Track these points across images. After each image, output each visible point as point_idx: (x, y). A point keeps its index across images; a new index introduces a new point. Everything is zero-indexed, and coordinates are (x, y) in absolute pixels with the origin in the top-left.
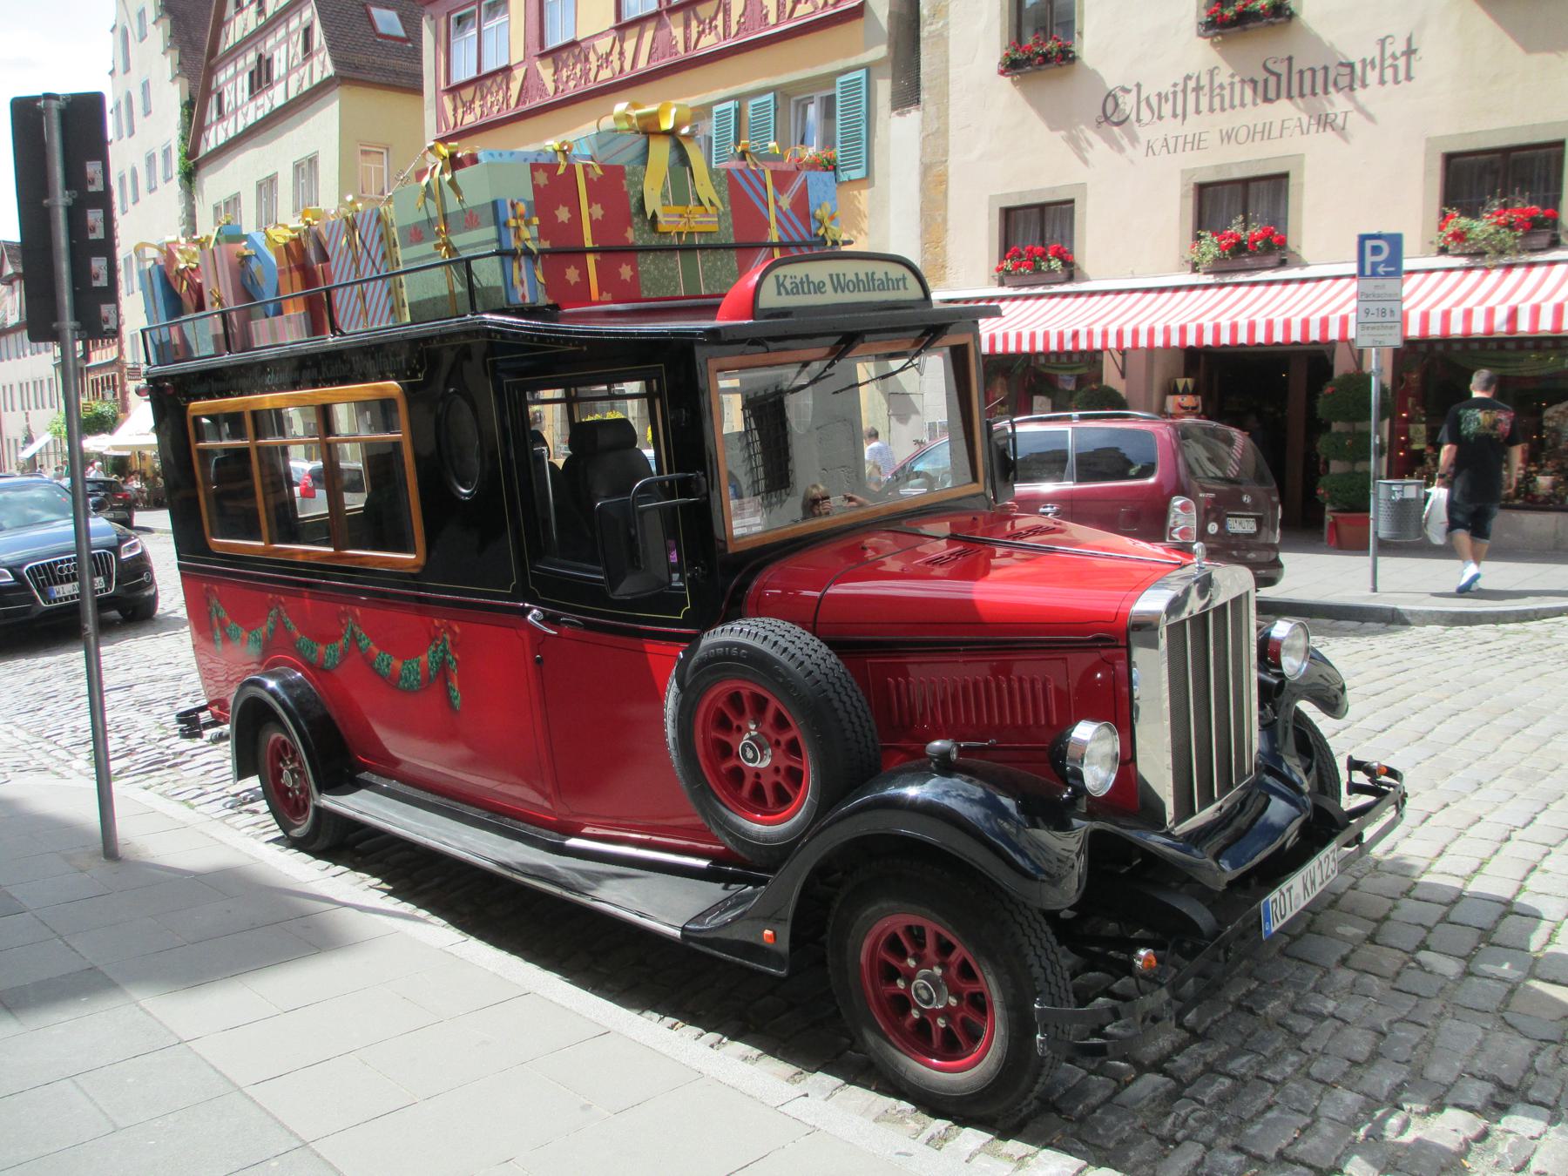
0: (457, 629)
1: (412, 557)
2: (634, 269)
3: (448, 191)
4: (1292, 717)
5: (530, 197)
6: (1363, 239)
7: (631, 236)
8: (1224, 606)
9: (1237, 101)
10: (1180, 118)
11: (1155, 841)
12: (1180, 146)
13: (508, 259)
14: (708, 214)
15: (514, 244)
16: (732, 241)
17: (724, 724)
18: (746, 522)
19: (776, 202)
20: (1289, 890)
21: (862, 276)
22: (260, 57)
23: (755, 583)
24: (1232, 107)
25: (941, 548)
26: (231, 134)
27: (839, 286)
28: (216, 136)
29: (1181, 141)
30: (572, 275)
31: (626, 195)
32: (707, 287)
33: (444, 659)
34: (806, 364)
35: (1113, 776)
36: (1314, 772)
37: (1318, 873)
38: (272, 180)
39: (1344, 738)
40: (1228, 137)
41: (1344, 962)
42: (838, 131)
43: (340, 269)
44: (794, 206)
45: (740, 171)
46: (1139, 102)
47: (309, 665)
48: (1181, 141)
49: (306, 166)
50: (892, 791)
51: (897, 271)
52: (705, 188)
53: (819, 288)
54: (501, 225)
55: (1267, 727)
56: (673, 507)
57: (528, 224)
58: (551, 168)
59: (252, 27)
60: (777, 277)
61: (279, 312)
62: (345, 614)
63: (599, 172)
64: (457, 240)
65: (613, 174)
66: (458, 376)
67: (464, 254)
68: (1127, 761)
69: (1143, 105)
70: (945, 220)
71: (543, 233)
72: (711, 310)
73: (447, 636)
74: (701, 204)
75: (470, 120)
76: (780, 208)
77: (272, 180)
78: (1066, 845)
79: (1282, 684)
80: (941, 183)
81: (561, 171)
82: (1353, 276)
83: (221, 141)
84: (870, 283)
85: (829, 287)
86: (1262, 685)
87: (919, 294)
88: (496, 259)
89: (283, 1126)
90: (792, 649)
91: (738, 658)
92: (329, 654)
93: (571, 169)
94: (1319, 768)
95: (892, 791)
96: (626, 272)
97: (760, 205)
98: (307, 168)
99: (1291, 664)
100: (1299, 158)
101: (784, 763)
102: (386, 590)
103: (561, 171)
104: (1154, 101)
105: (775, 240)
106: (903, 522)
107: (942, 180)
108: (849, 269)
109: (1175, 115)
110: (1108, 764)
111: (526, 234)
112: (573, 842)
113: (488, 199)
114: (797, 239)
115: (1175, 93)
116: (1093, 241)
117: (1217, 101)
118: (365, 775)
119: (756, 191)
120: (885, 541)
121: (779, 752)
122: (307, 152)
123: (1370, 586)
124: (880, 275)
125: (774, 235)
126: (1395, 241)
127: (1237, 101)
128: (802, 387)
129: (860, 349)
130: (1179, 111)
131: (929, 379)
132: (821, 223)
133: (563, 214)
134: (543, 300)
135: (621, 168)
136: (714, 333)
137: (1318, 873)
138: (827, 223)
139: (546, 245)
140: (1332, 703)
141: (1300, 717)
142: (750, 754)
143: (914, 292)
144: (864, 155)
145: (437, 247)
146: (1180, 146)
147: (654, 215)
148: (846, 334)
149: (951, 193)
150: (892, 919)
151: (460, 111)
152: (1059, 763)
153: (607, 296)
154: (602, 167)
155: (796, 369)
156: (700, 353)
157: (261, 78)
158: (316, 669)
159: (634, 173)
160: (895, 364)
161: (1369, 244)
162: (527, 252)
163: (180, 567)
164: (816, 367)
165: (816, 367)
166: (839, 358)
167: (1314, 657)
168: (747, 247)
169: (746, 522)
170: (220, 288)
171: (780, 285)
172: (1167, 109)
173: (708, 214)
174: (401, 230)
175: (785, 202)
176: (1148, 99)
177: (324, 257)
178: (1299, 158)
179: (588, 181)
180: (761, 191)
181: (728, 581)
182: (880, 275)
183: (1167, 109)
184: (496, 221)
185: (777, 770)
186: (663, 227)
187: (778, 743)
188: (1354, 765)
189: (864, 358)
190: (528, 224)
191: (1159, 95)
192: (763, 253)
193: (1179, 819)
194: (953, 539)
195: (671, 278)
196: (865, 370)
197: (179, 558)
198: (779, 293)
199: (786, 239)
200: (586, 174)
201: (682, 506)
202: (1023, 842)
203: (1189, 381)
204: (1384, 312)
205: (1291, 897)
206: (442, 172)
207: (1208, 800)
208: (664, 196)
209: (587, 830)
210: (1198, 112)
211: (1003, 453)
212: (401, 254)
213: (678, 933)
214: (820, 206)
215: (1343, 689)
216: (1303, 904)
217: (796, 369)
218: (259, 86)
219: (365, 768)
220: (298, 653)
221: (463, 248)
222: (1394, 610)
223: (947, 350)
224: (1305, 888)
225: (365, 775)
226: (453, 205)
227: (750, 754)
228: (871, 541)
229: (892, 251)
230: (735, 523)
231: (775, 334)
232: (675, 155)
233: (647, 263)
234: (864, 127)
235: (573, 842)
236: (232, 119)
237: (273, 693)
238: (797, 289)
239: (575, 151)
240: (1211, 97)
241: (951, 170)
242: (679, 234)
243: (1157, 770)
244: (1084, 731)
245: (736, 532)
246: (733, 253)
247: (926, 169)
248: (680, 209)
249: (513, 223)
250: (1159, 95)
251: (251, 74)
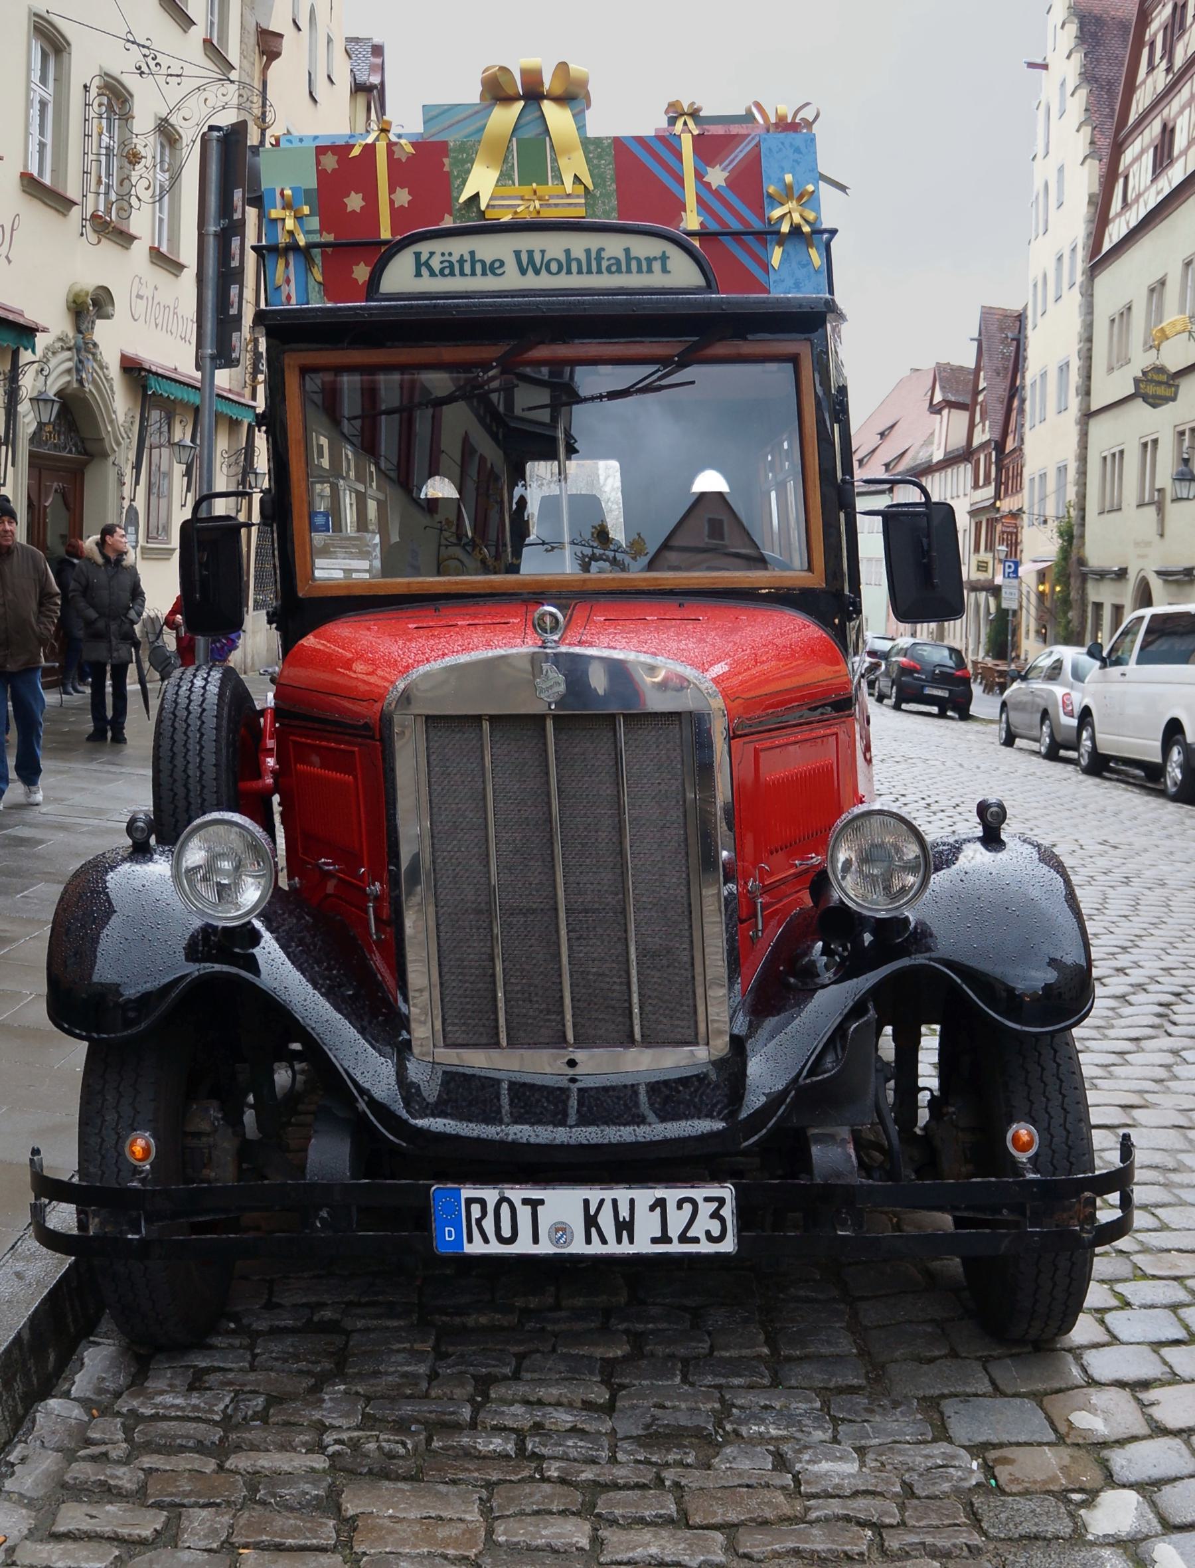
5: (313, 184)
19: (699, 176)
22: (1165, 126)
28: (1116, 231)
44: (731, 183)
53: (494, 268)
58: (341, 150)
59: (1160, 87)
60: (418, 255)
89: (1138, 1343)
93: (370, 149)
103: (356, 152)
114: (736, 226)
133: (355, 202)
135: (445, 144)
139: (329, 238)
154: (414, 145)
157: (1163, 155)
162: (293, 247)
175: (717, 177)
198: (418, 274)
199: (713, 227)
202: (422, 936)
218: (1161, 165)
238: (449, 270)
251: (1156, 148)
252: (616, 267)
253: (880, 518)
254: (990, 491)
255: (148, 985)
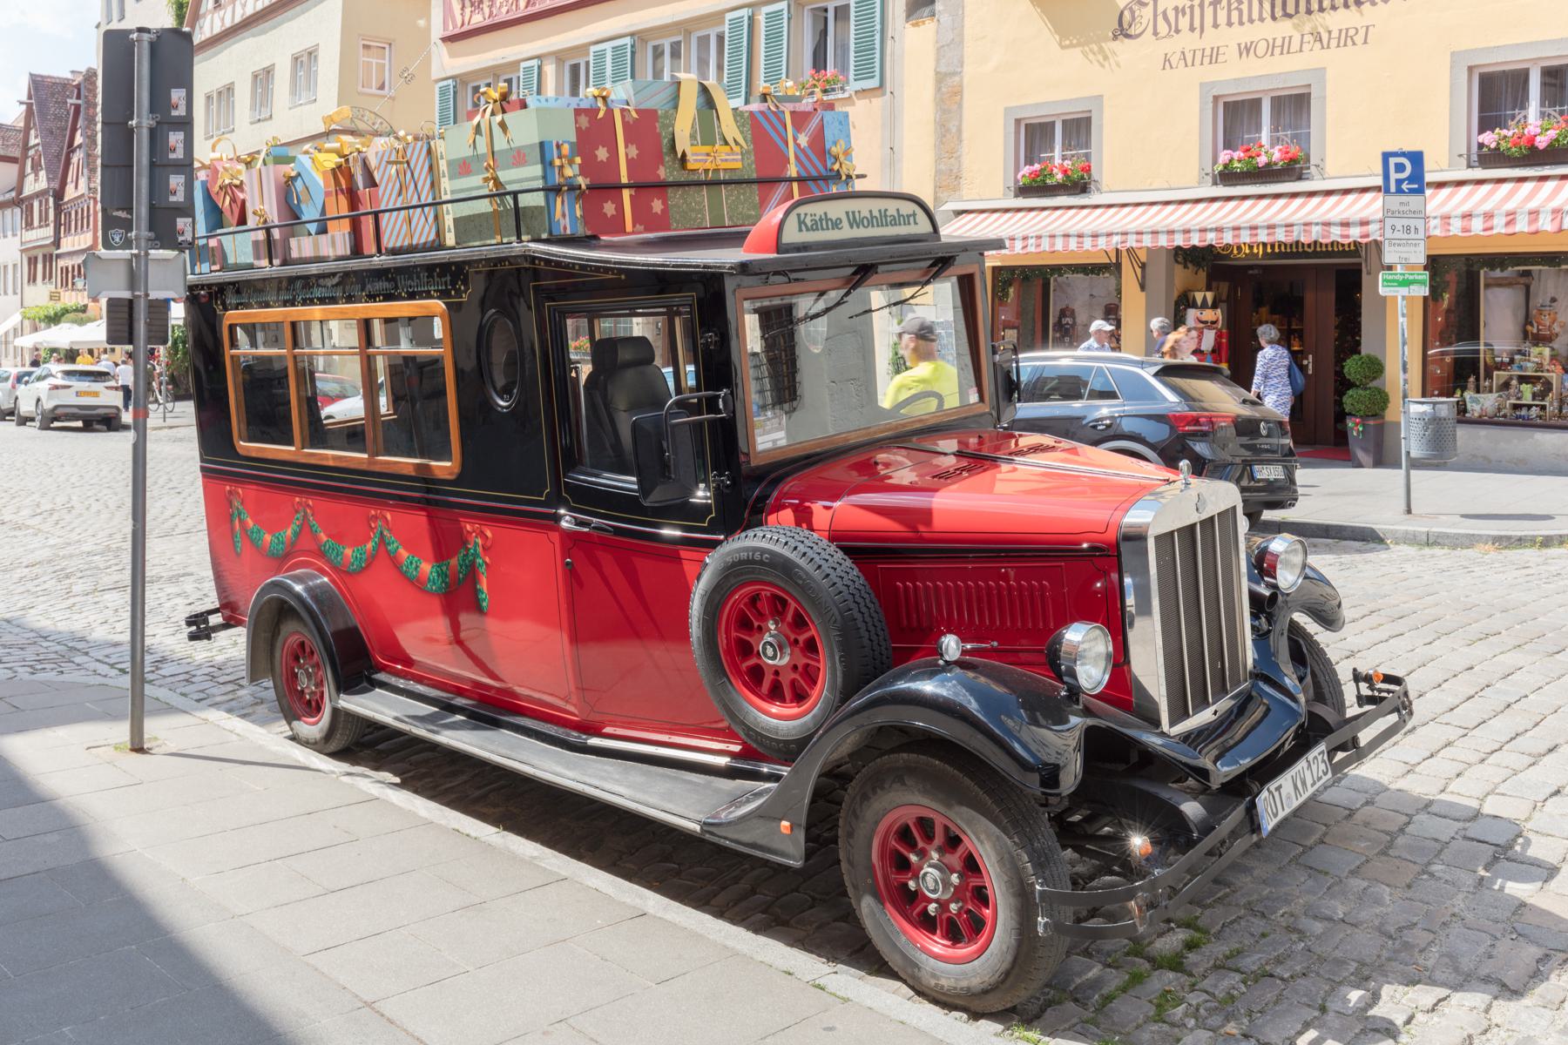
0: (489, 534)
1: (448, 464)
2: (665, 203)
3: (497, 130)
4: (1290, 635)
5: (574, 139)
6: (1386, 156)
7: (663, 173)
8: (1212, 518)
9: (1255, 15)
10: (1198, 31)
11: (1153, 740)
12: (1198, 61)
13: (552, 195)
14: (731, 156)
15: (558, 180)
16: (754, 176)
17: (745, 624)
18: (769, 436)
19: (795, 139)
20: (1278, 789)
21: (876, 213)
23: (775, 494)
24: (1251, 21)
25: (950, 462)
26: (228, 24)
27: (854, 222)
29: (1198, 54)
30: (609, 208)
31: (659, 135)
32: (730, 218)
33: (473, 564)
34: (822, 294)
35: (1107, 677)
36: (1309, 678)
37: (1308, 774)
38: (268, 72)
39: (1348, 650)
40: (1246, 50)
41: (1354, 873)
42: (852, 41)
43: (387, 196)
44: (811, 144)
45: (762, 113)
46: (1155, 16)
47: (335, 569)
48: (1198, 54)
49: (305, 59)
50: (902, 685)
51: (907, 208)
52: (729, 128)
53: (836, 224)
54: (546, 163)
55: (1261, 637)
56: (701, 423)
57: (571, 163)
61: (323, 230)
62: (376, 518)
63: (634, 115)
64: (503, 176)
65: (648, 116)
66: (510, 296)
67: (510, 188)
68: (1120, 660)
69: (1160, 19)
70: (960, 131)
71: (584, 171)
72: (737, 238)
73: (479, 541)
74: (726, 143)
75: (478, 20)
76: (798, 145)
77: (268, 72)
78: (1063, 742)
79: (1274, 597)
80: (955, 94)
81: (601, 115)
82: (1378, 189)
83: (217, 30)
84: (883, 219)
85: (845, 223)
86: (1255, 598)
87: (928, 228)
88: (541, 194)
90: (810, 553)
91: (761, 562)
92: (351, 554)
93: (610, 112)
94: (1314, 674)
95: (902, 685)
96: (657, 206)
97: (781, 144)
98: (305, 61)
99: (1287, 578)
100: (1321, 72)
101: (802, 661)
102: (424, 495)
103: (601, 115)
104: (1171, 15)
105: (794, 175)
106: (913, 436)
107: (958, 92)
108: (864, 207)
109: (1192, 29)
110: (1102, 664)
111: (569, 172)
112: (595, 741)
113: (537, 141)
114: (815, 174)
115: (1192, 7)
116: (1111, 160)
117: (1235, 14)
118: (382, 676)
119: (777, 131)
120: (899, 457)
121: (797, 651)
122: (308, 44)
123: (1403, 507)
124: (892, 212)
125: (793, 170)
126: (1417, 158)
127: (1255, 15)
128: (817, 316)
129: (874, 278)
130: (1197, 23)
131: (937, 303)
132: (836, 158)
133: (602, 154)
134: (581, 231)
135: (654, 112)
136: (744, 268)
137: (1308, 774)
138: (842, 158)
140: (1328, 617)
141: (1294, 628)
142: (770, 651)
143: (923, 227)
144: (878, 55)
145: (486, 180)
146: (1198, 61)
147: (684, 154)
148: (860, 269)
149: (966, 104)
150: (905, 803)
151: (468, 10)
152: (1055, 663)
153: (640, 227)
154: (637, 111)
155: (814, 296)
156: (729, 285)
158: (342, 572)
159: (666, 115)
160: (908, 292)
161: (1392, 161)
162: (573, 188)
163: (203, 469)
164: (834, 295)
165: (834, 295)
166: (854, 287)
167: (1312, 577)
168: (767, 182)
169: (769, 436)
170: (264, 205)
171: (801, 223)
172: (1184, 23)
173: (730, 154)
174: (449, 163)
175: (803, 140)
176: (1164, 13)
177: (372, 183)
178: (1321, 72)
179: (625, 124)
180: (781, 129)
181: (749, 492)
182: (892, 212)
183: (1184, 23)
184: (543, 161)
185: (795, 668)
186: (690, 166)
187: (796, 641)
188: (1357, 677)
189: (878, 286)
190: (571, 163)
191: (1176, 9)
192: (781, 189)
193: (1172, 724)
194: (959, 454)
195: (699, 210)
196: (877, 297)
197: (202, 460)
199: (804, 174)
200: (623, 117)
201: (710, 422)
202: (1025, 736)
203: (1210, 296)
204: (1408, 229)
205: (1279, 800)
206: (493, 114)
207: (1202, 703)
208: (693, 137)
209: (608, 730)
210: (1216, 26)
211: (1008, 374)
212: (445, 184)
213: (698, 828)
214: (835, 143)
215: (1339, 605)
216: (1296, 804)
217: (814, 296)
219: (384, 668)
220: (321, 554)
221: (510, 182)
222: (1373, 531)
223: (954, 279)
224: (1296, 787)
225: (382, 676)
226: (500, 143)
227: (770, 651)
228: (882, 457)
229: (906, 189)
230: (759, 440)
231: (795, 266)
232: (702, 100)
233: (675, 196)
234: (878, 37)
235: (595, 741)
236: (230, 9)
237: (298, 596)
238: (815, 227)
239: (612, 97)
240: (1229, 11)
241: (966, 81)
242: (706, 171)
243: (1149, 667)
244: (1077, 635)
245: (760, 447)
246: (755, 187)
247: (940, 78)
248: (707, 149)
249: (557, 162)
250: (1176, 9)
252: (895, 222)
253: (596, 322)
254: (49, 231)
255: (1444, 564)
